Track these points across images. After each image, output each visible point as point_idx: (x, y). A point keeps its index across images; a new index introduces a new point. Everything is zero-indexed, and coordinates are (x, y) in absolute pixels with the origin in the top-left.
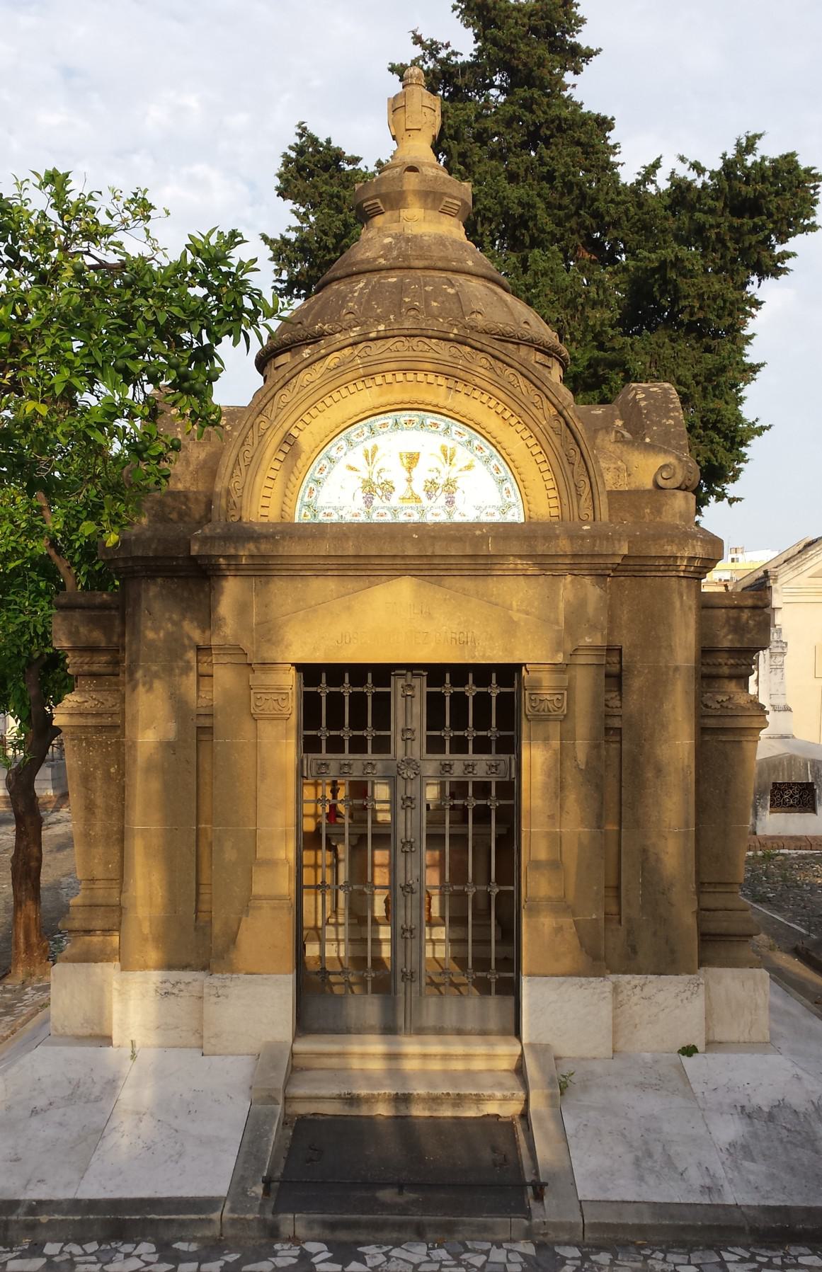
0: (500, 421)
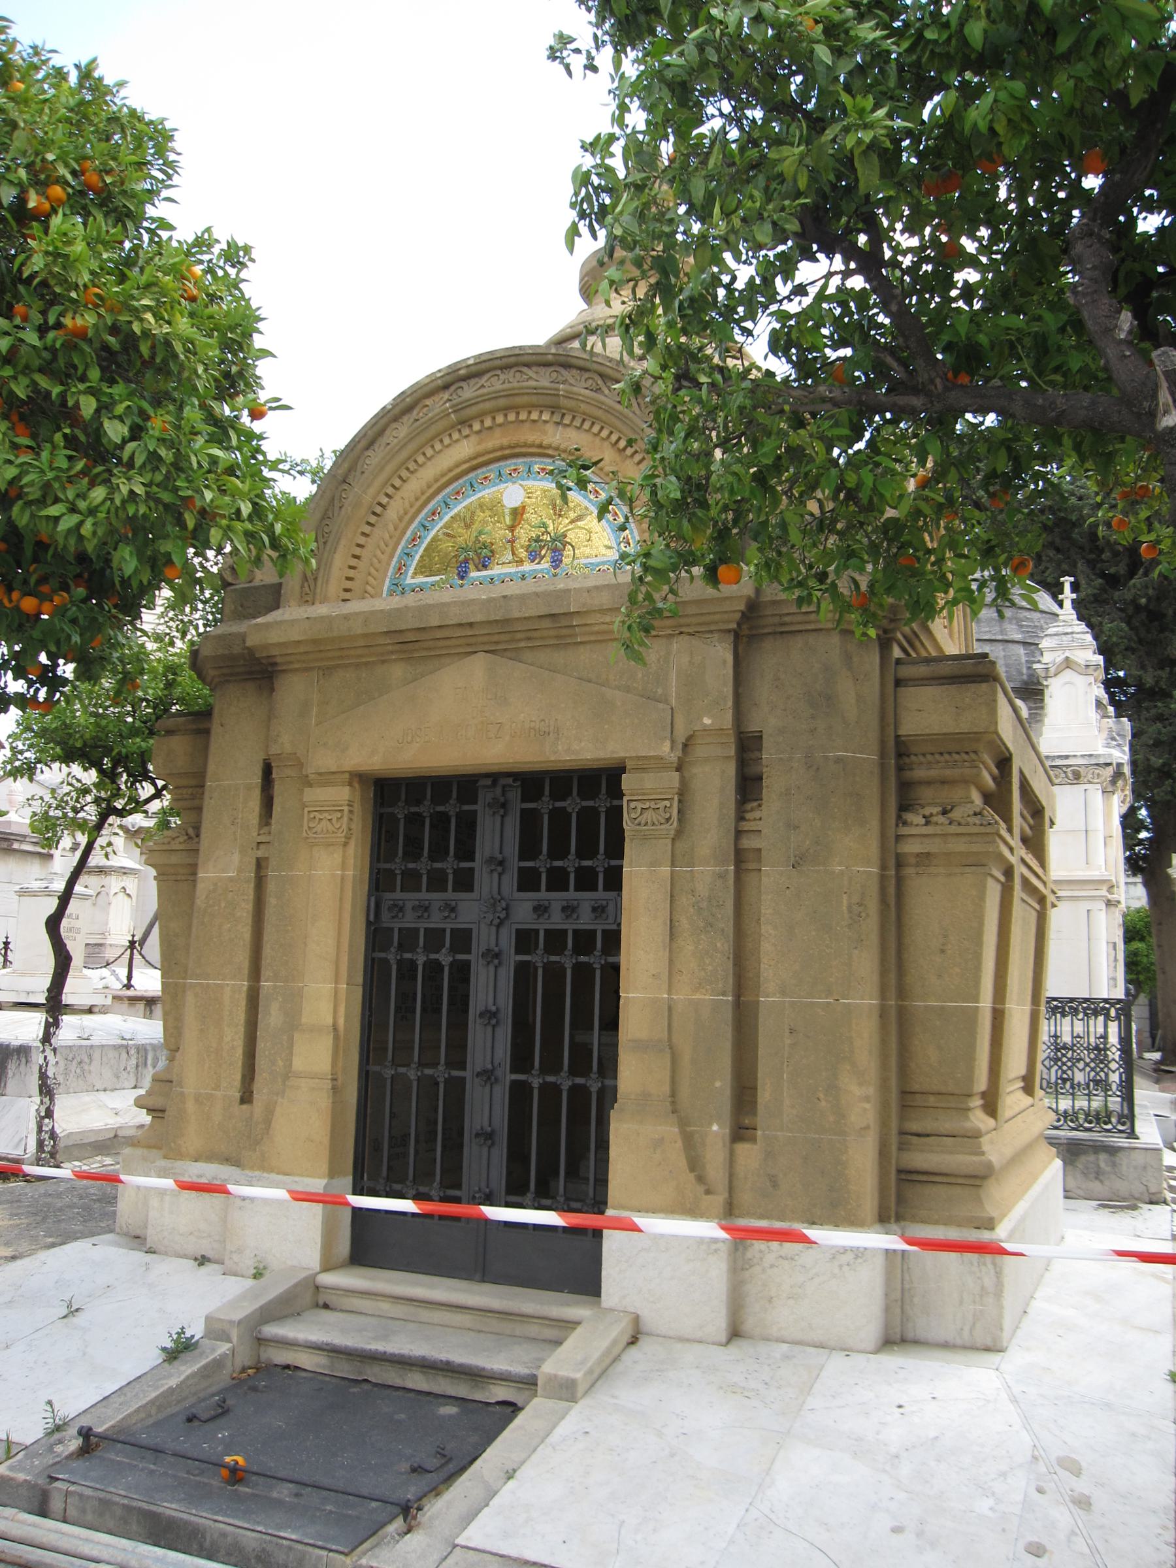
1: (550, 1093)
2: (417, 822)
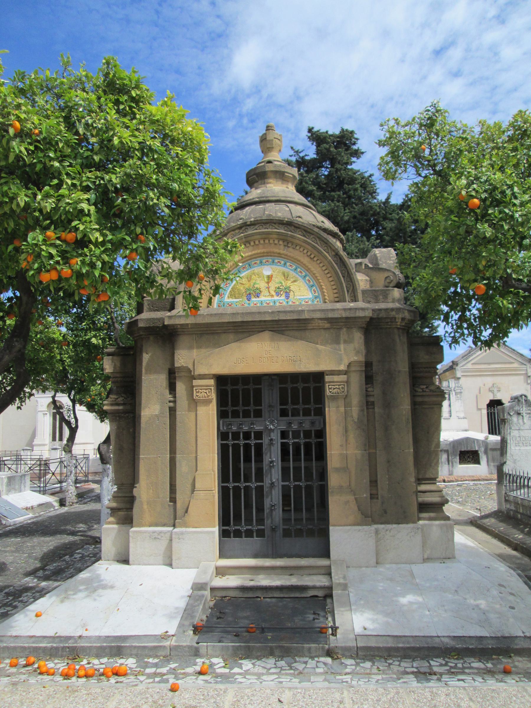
0: (309, 259)
1: (237, 490)
2: (237, 394)
